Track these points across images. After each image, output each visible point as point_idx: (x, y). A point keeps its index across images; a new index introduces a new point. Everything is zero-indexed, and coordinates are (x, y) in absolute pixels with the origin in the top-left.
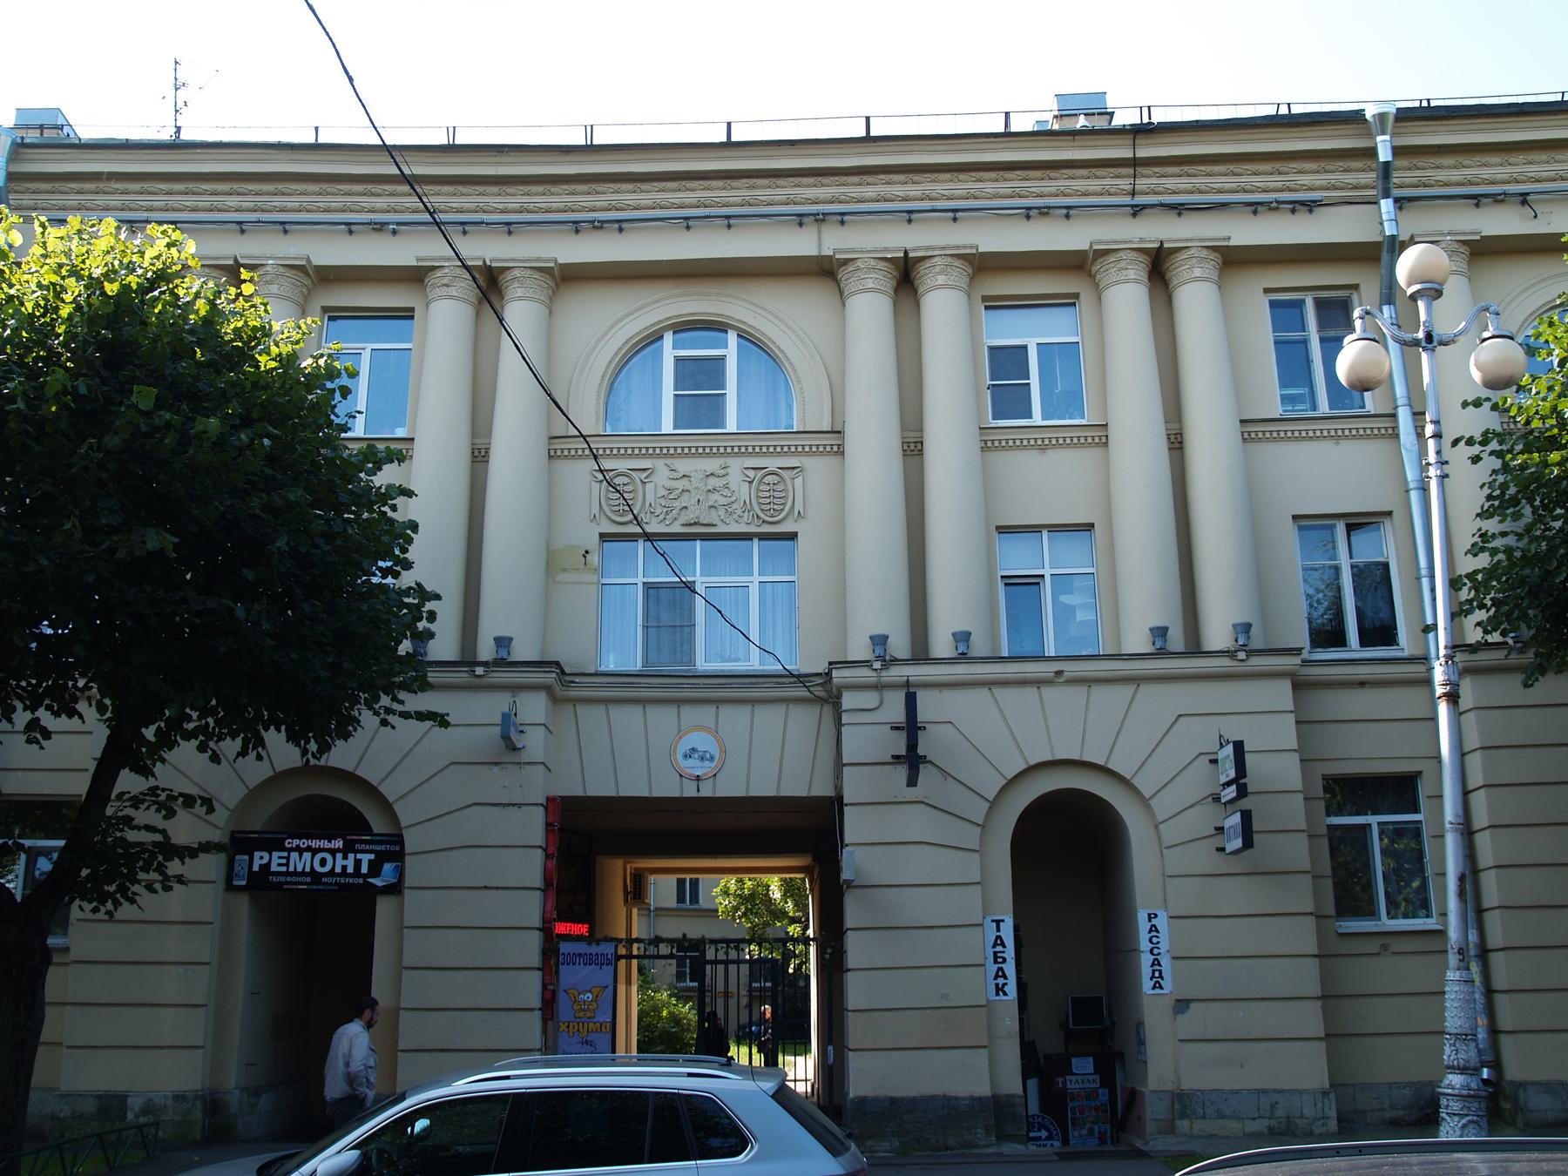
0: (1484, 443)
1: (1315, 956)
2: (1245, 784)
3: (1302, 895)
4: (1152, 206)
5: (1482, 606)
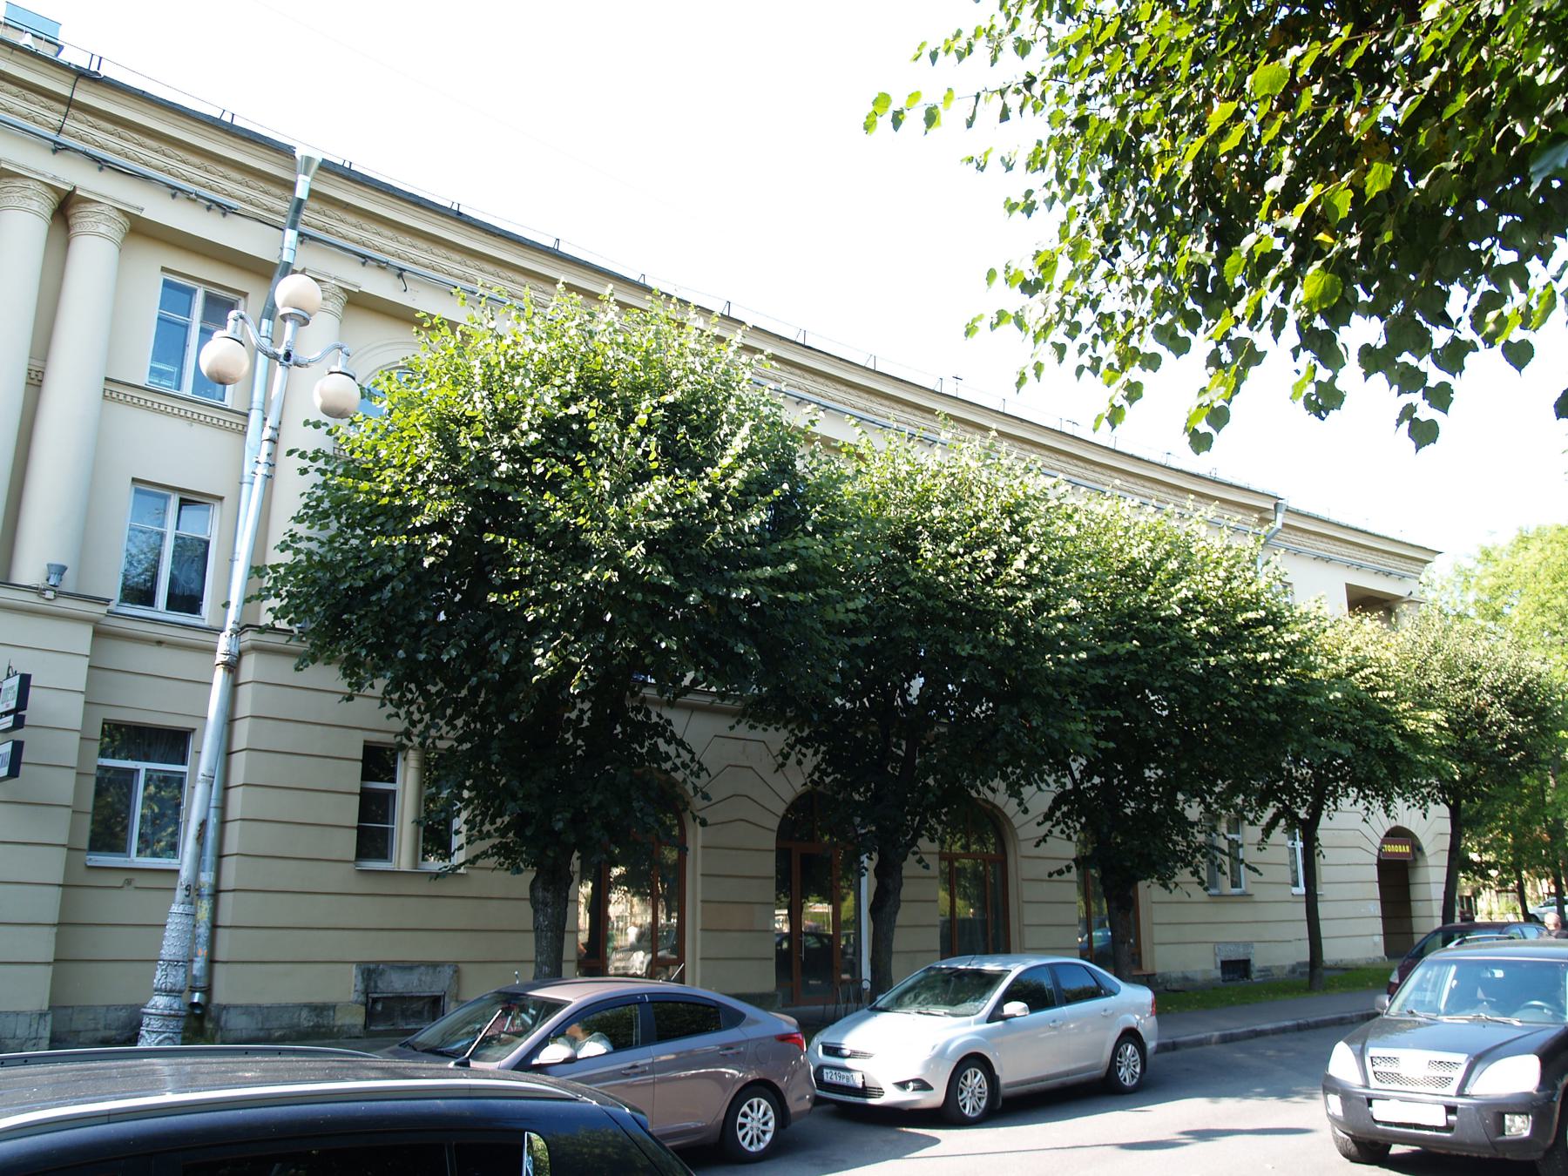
0: (313, 459)
1: (59, 885)
2: (24, 717)
3: (58, 828)
4: (76, 151)
5: (277, 595)
